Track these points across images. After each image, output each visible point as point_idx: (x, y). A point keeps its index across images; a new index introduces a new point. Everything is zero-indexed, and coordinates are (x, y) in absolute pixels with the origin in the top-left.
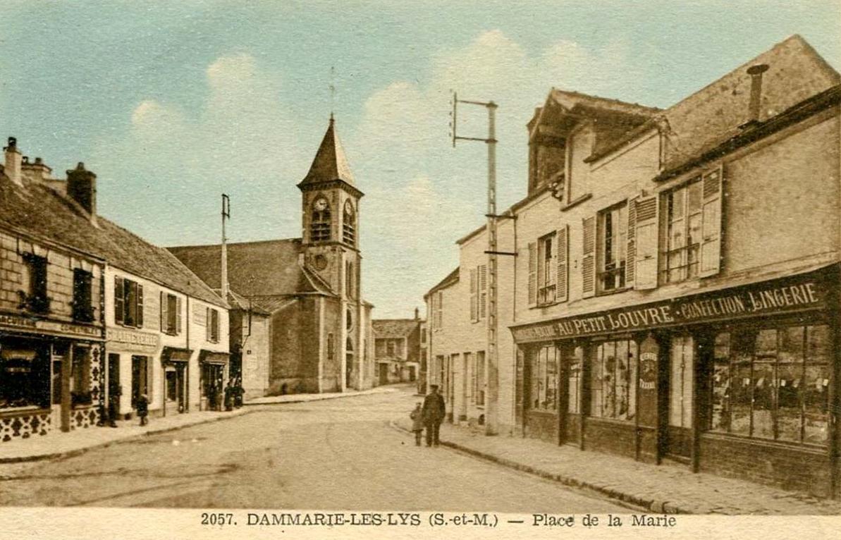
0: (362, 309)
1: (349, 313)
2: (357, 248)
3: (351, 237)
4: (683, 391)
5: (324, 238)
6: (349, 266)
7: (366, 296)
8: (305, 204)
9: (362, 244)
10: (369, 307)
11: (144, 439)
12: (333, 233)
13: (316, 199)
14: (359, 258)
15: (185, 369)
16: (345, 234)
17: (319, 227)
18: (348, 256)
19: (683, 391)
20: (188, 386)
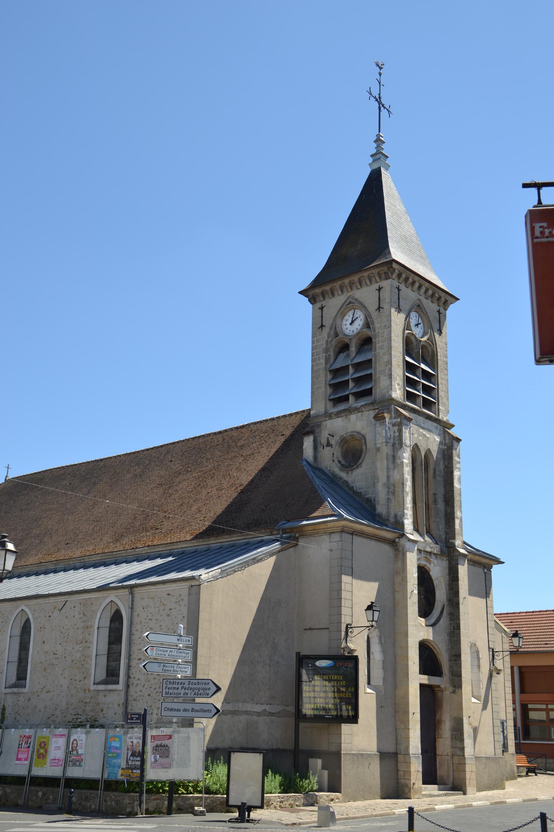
0: (463, 570)
1: (424, 576)
2: (442, 417)
3: (427, 390)
4: (127, 700)
5: (359, 395)
6: (421, 462)
7: (473, 530)
8: (319, 326)
9: (455, 404)
10: (484, 563)
11: (202, 544)
12: (383, 382)
13: (341, 314)
14: (450, 444)
15: (110, 585)
16: (409, 382)
17: (347, 371)
18: (419, 436)
19: (127, 700)
20: (247, 564)
